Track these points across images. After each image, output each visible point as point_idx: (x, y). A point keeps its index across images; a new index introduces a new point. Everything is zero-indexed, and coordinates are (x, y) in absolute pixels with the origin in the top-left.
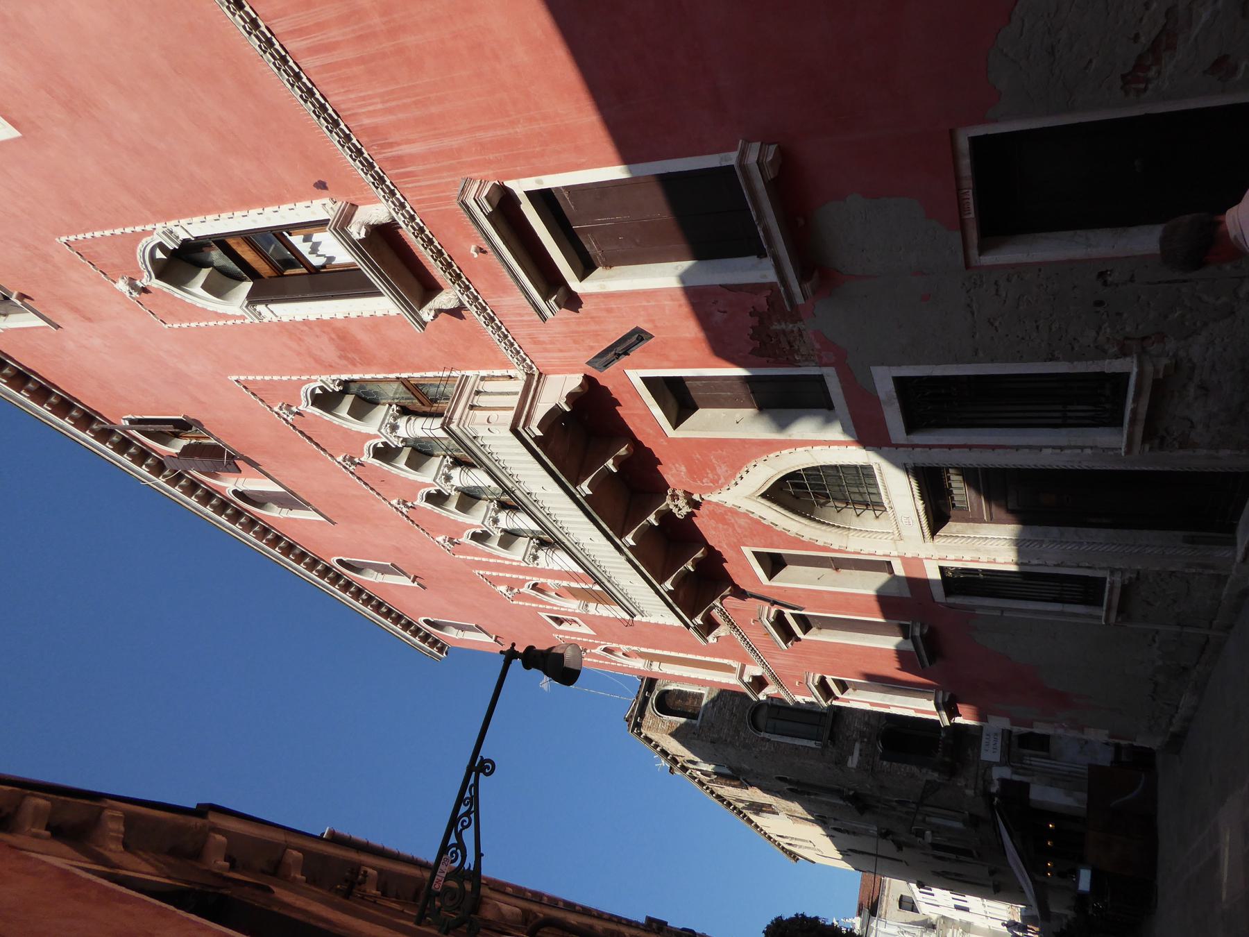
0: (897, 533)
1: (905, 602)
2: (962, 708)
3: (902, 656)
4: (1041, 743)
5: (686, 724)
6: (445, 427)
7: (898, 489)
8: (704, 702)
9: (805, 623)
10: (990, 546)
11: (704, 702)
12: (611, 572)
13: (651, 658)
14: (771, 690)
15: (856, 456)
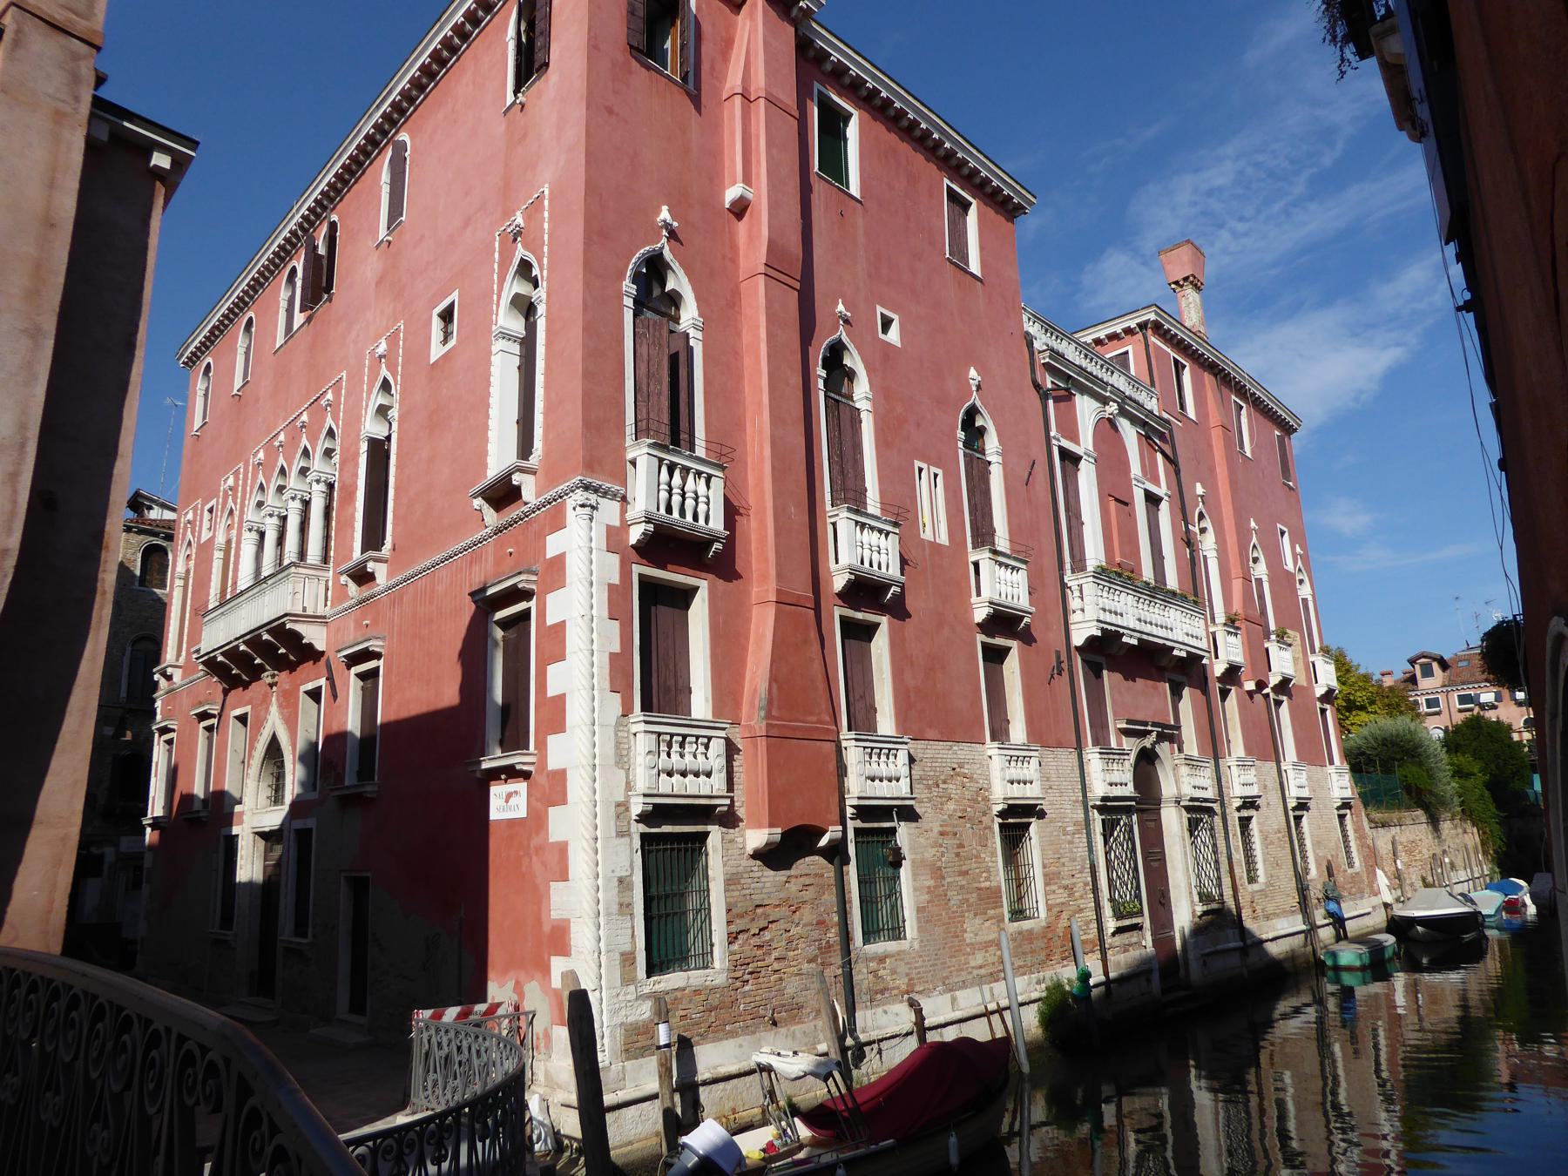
0: (258, 813)
1: (220, 807)
2: (157, 833)
3: (188, 798)
4: (137, 884)
5: (134, 575)
6: (292, 564)
7: (274, 818)
8: (157, 591)
9: (209, 729)
10: (249, 867)
11: (157, 591)
12: (232, 617)
13: (186, 579)
14: (163, 683)
15: (288, 799)
